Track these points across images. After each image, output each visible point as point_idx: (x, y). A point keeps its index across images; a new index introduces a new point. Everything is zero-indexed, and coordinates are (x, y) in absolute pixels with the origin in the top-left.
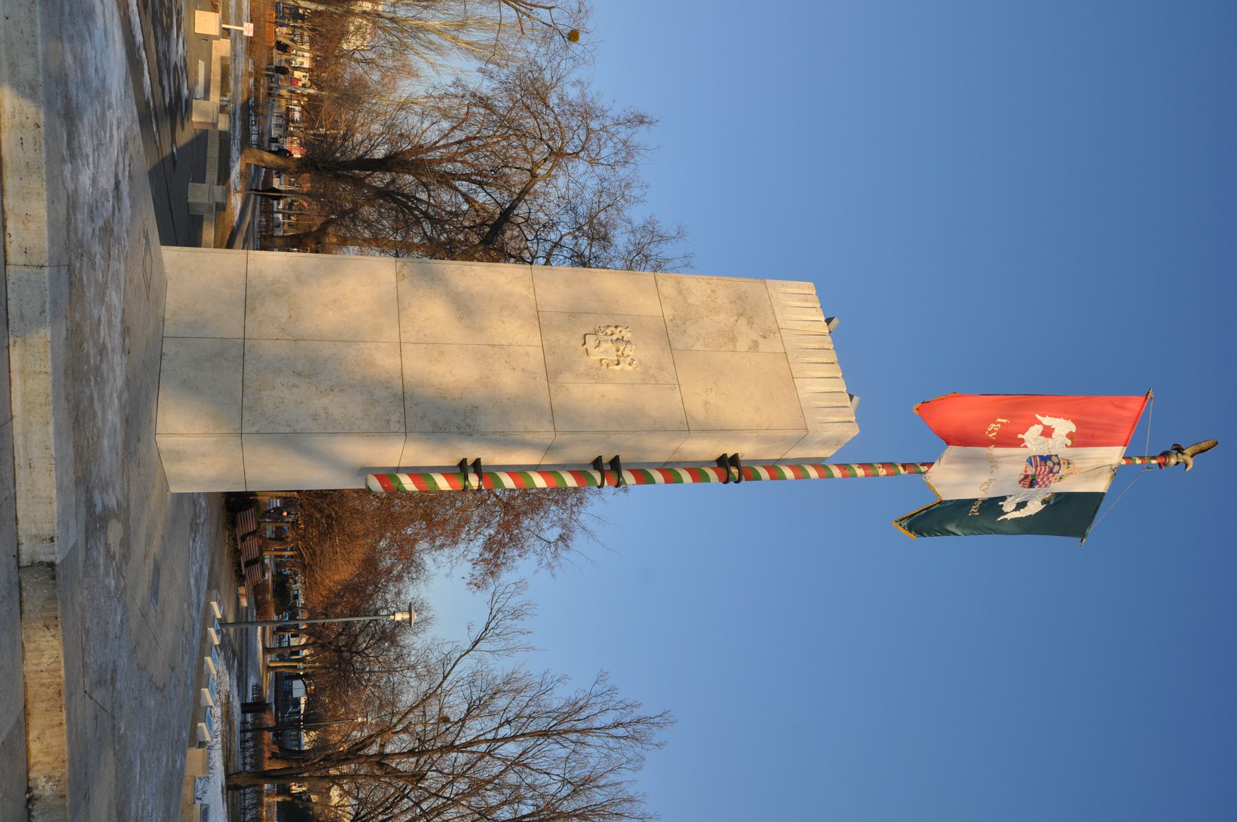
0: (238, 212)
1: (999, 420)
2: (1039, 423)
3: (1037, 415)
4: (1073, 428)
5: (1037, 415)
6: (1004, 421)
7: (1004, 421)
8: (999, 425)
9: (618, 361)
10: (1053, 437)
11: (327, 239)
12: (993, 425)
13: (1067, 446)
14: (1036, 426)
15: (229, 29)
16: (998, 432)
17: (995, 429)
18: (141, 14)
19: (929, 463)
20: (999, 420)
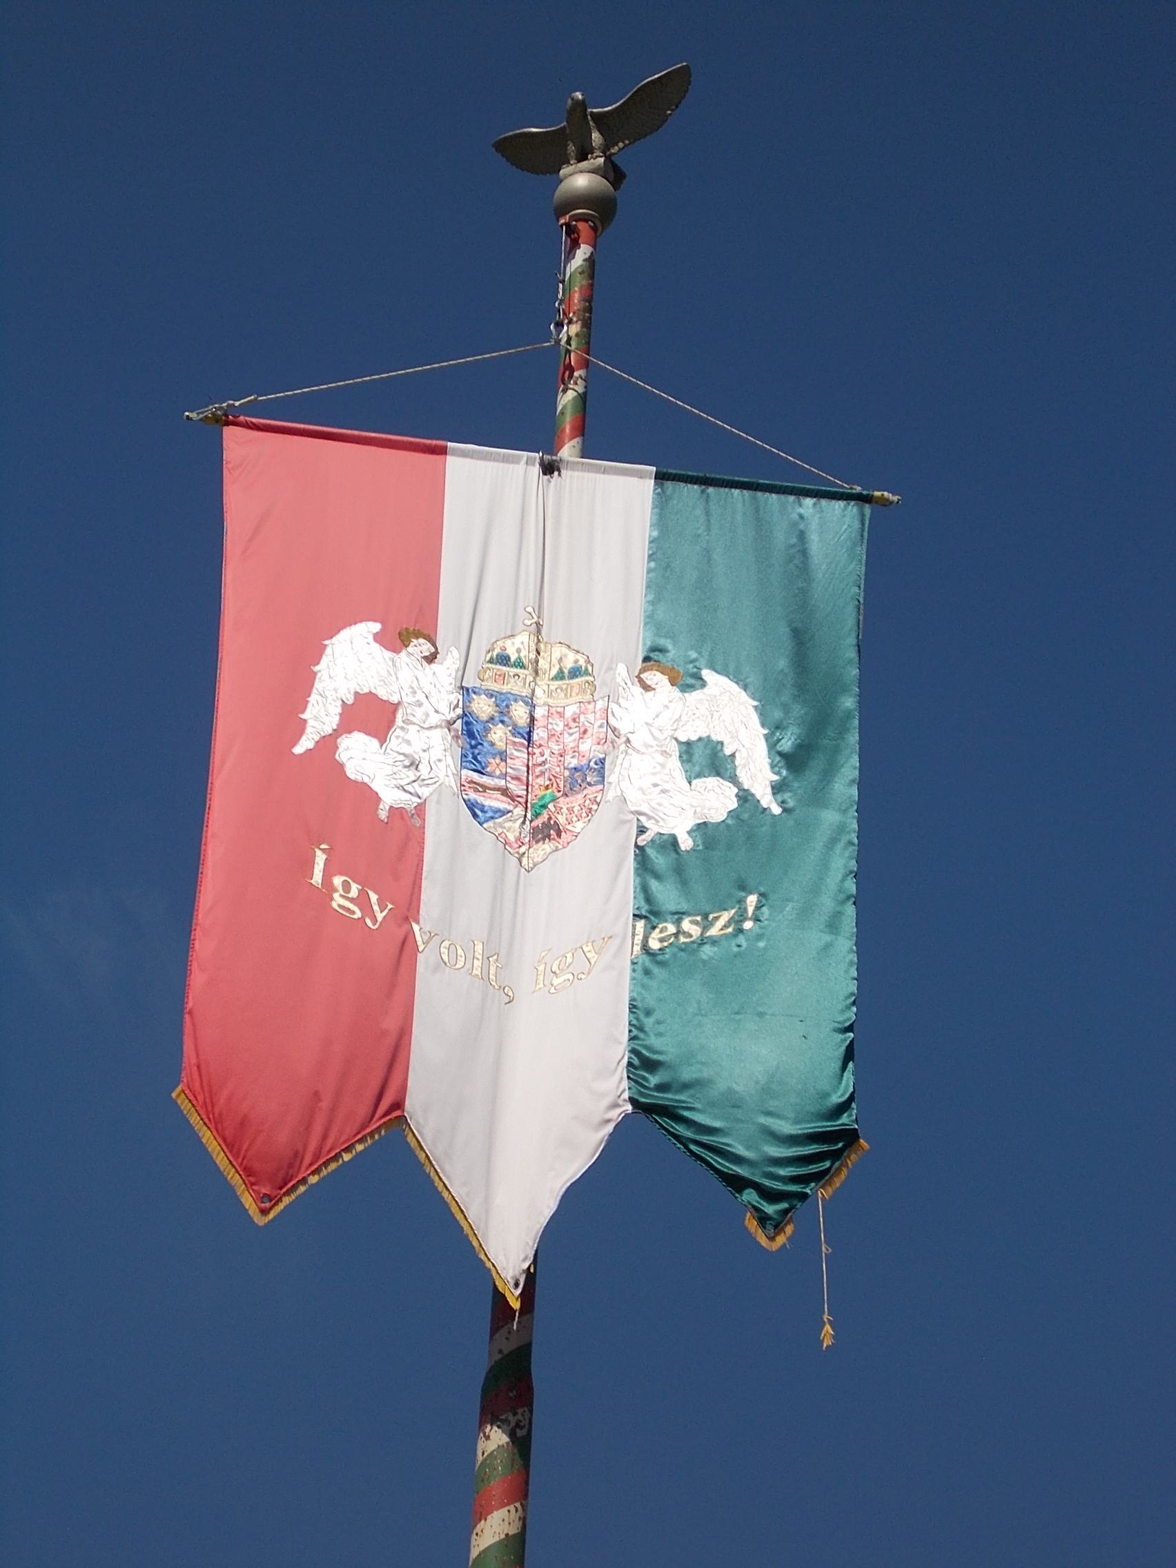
0: (721, 1140)
1: (317, 878)
2: (328, 744)
3: (298, 750)
4: (376, 627)
5: (298, 750)
6: (320, 858)
7: (320, 858)
8: (338, 881)
9: (514, 676)
10: (395, 699)
11: (489, 1427)
12: (338, 900)
13: (431, 659)
14: (342, 755)
15: (582, 458)
16: (365, 884)
17: (354, 893)
18: (417, 1144)
19: (589, 349)
20: (317, 878)
